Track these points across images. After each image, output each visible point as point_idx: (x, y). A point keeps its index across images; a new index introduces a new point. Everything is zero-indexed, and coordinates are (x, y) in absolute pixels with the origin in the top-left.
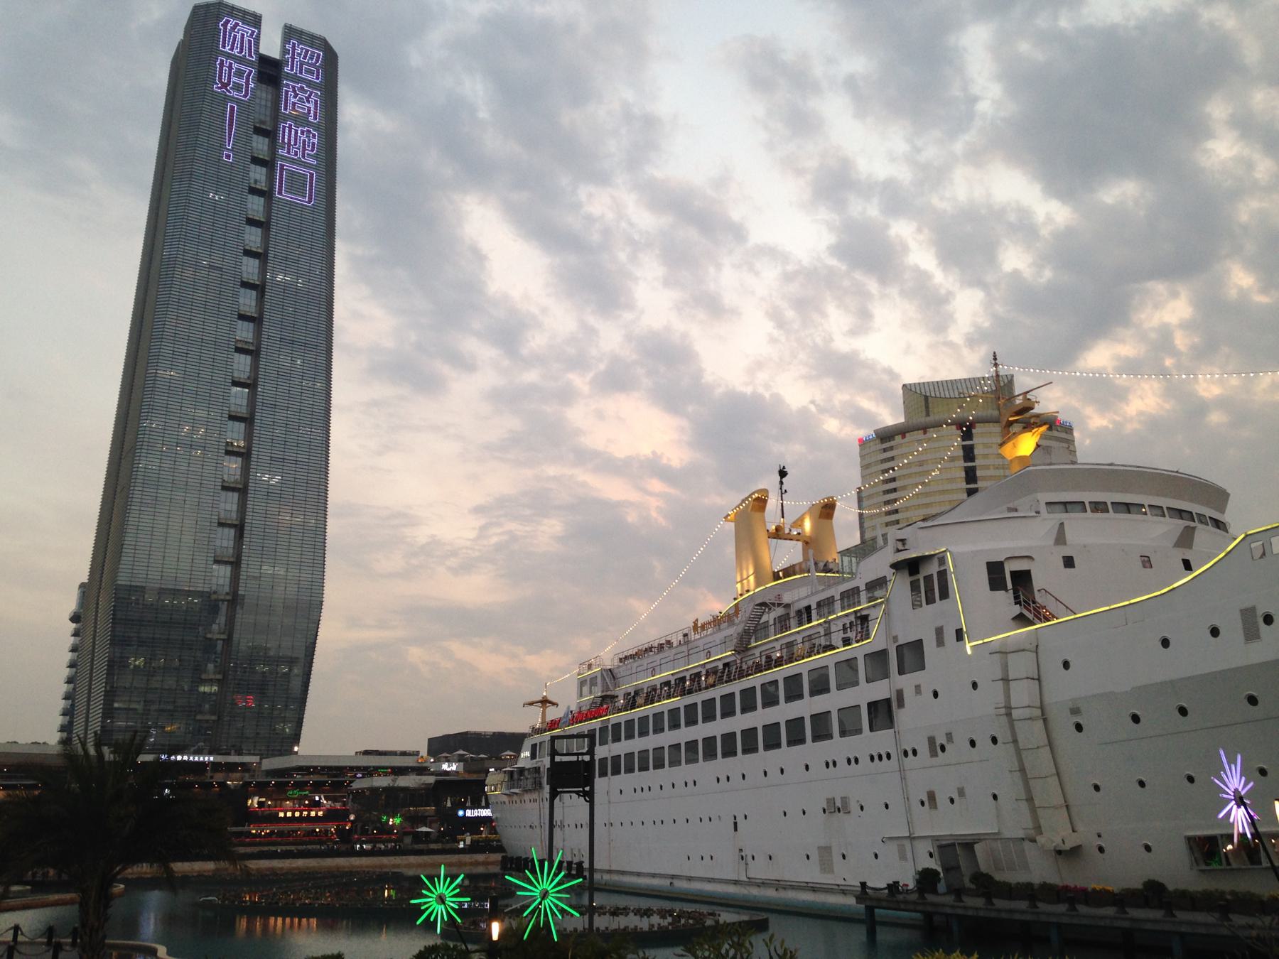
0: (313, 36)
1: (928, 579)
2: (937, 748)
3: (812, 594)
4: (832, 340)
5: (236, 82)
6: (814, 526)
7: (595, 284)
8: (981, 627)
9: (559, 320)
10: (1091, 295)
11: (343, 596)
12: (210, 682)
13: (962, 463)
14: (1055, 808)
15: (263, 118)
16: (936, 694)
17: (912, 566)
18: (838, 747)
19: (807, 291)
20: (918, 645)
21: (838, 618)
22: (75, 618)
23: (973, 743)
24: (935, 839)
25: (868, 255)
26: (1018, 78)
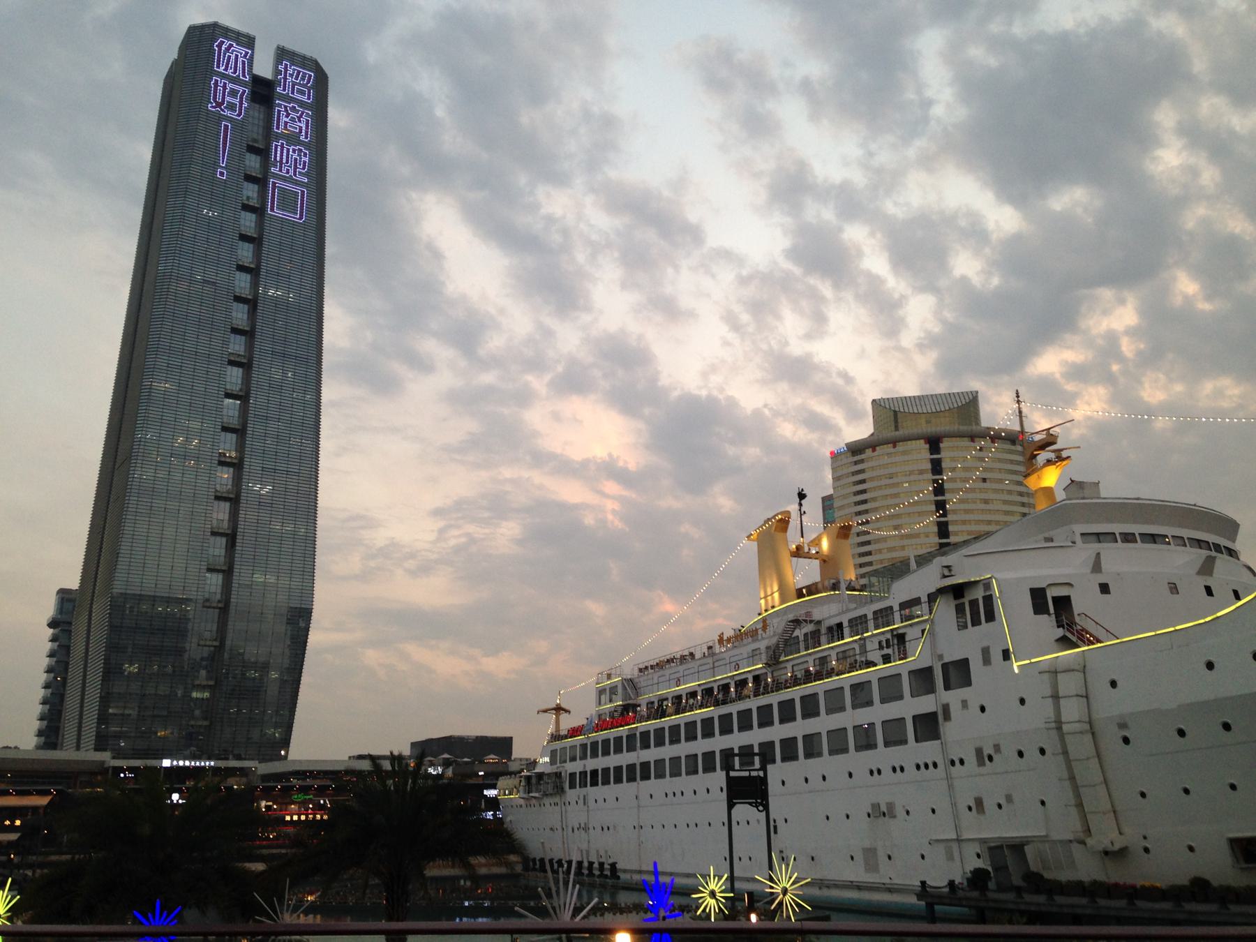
0: (304, 57)
1: (974, 603)
2: (983, 758)
3: (843, 612)
4: (787, 343)
5: (231, 102)
6: (832, 545)
7: (554, 286)
8: (1031, 651)
9: (517, 320)
10: (1038, 301)
11: (331, 599)
12: (202, 688)
13: (930, 476)
14: (1104, 813)
15: (255, 136)
16: (983, 709)
17: (958, 591)
18: (882, 756)
19: (763, 296)
20: (963, 665)
21: (873, 635)
22: (52, 624)
23: (1021, 754)
24: (983, 841)
25: (822, 258)
26: (972, 85)
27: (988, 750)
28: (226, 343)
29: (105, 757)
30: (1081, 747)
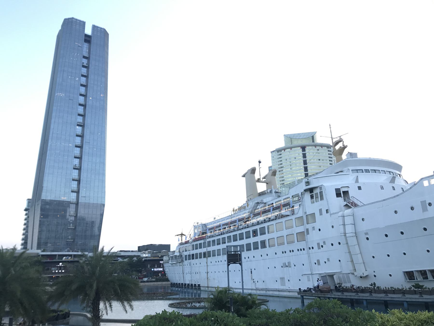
17: (311, 190)
22: (26, 210)
24: (320, 274)
27: (322, 244)
28: (76, 119)
29: (39, 252)
30: (353, 241)
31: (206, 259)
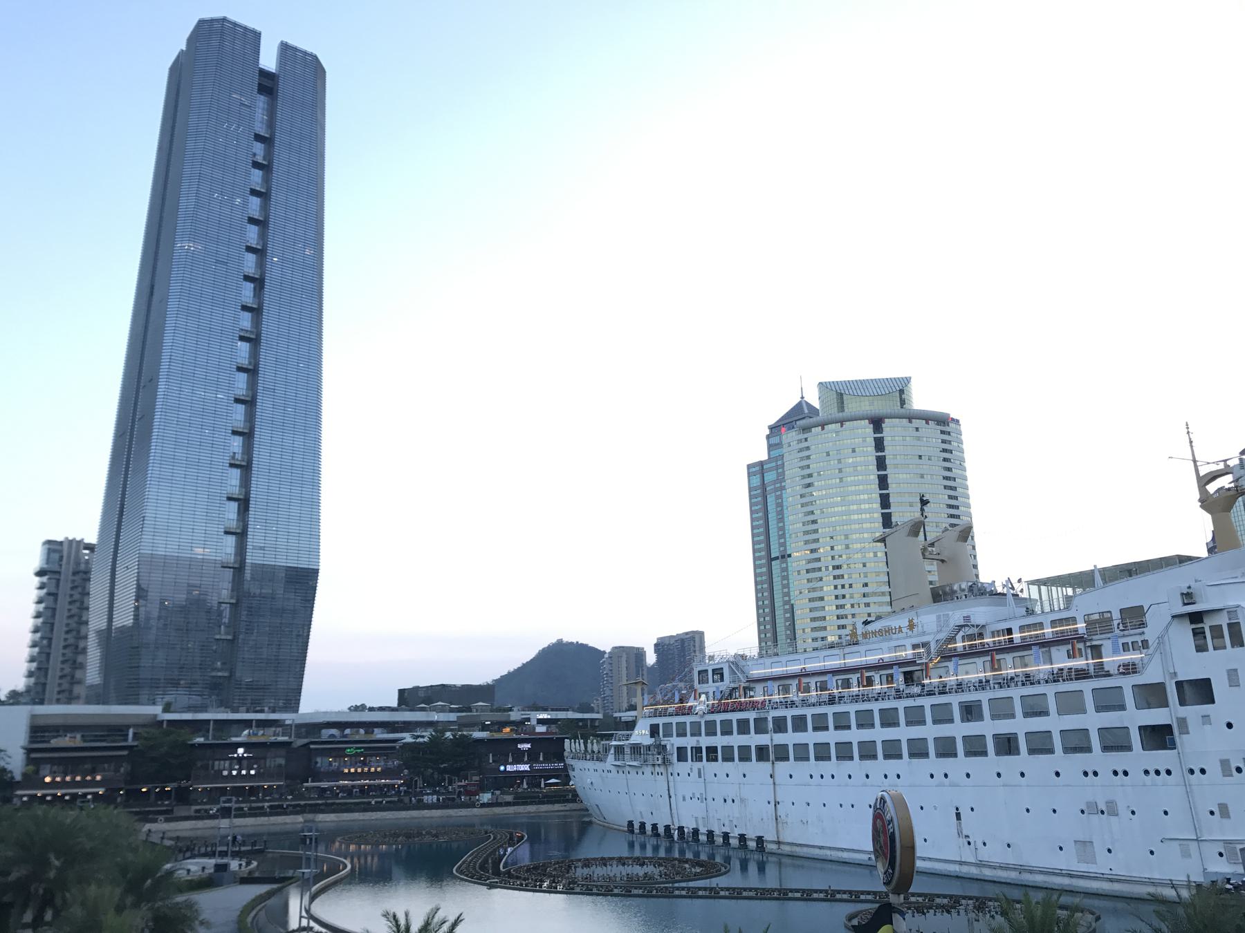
17: (1196, 617)
22: (40, 573)
31: (768, 765)
